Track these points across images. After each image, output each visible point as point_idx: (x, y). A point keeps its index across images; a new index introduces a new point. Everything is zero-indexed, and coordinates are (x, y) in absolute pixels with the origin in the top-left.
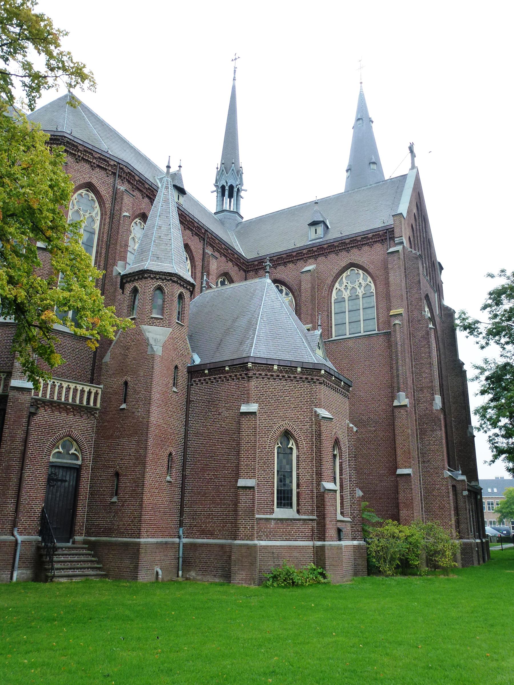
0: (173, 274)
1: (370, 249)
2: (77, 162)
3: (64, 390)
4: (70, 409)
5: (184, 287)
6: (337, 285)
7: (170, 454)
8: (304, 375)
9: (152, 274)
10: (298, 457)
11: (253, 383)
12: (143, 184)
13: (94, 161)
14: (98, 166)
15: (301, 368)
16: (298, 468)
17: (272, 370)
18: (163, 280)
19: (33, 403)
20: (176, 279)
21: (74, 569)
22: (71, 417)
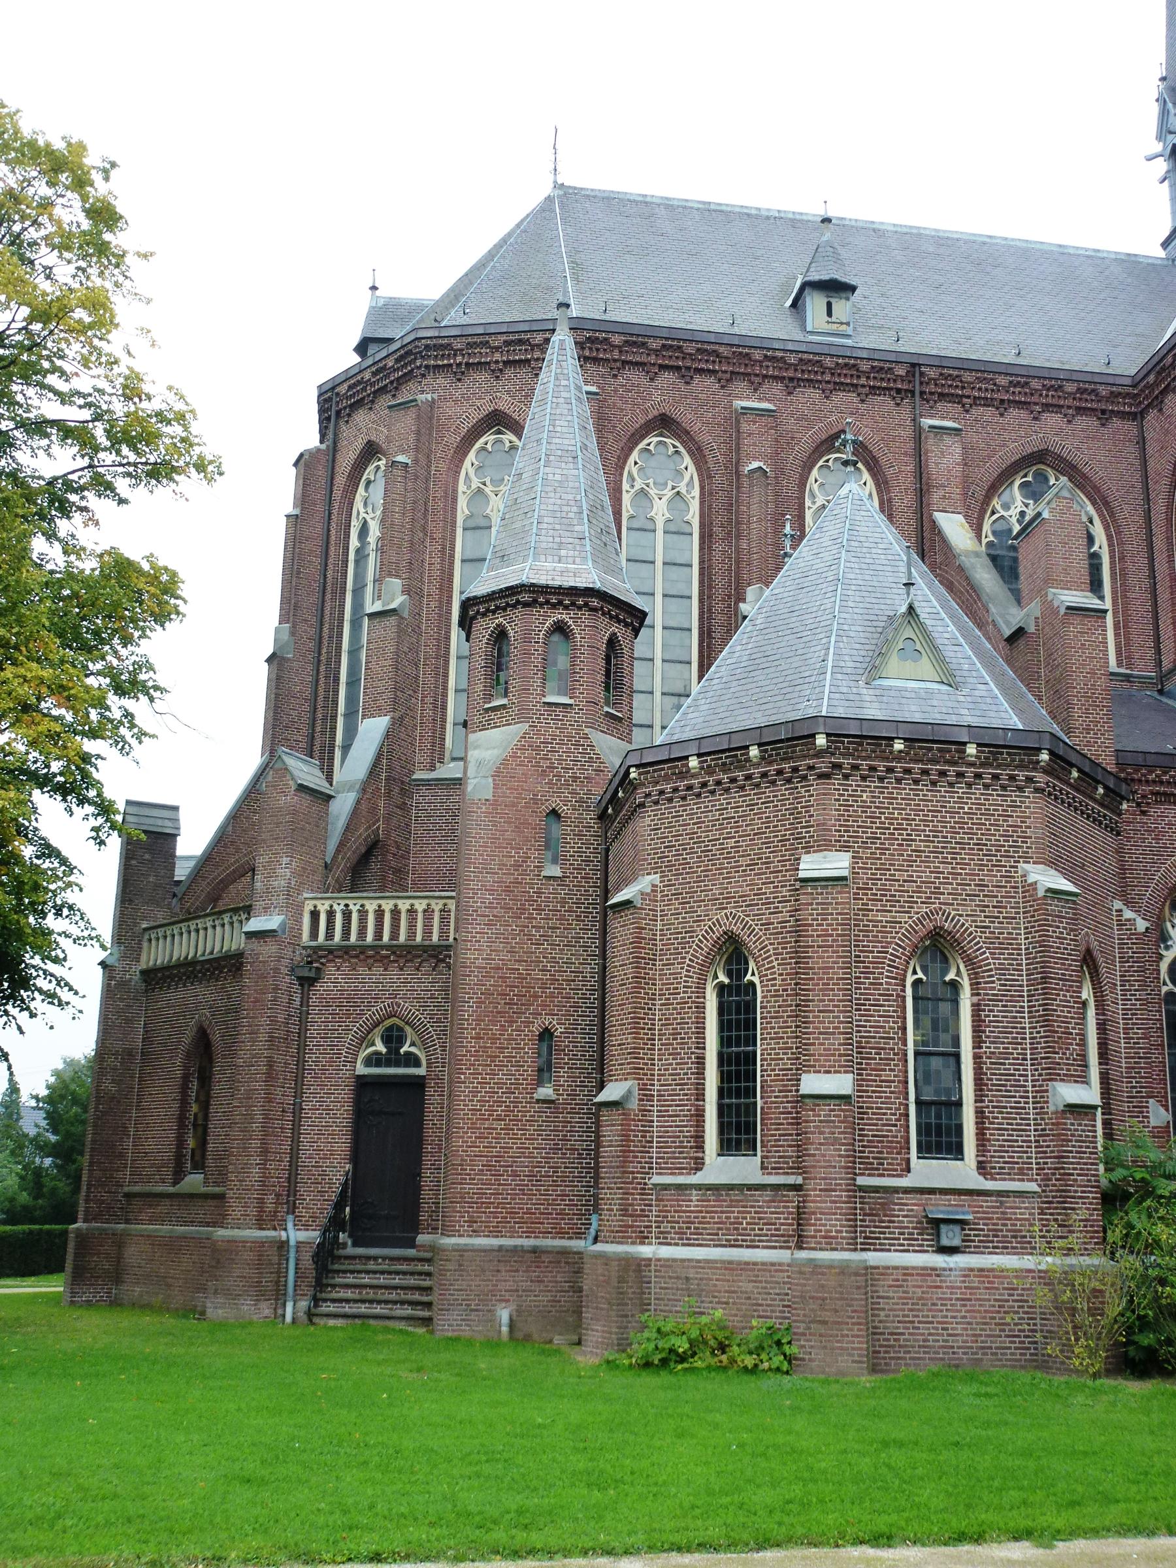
0: (517, 586)
1: (644, 381)
2: (459, 380)
3: (371, 918)
4: (388, 957)
5: (619, 621)
6: (996, 503)
7: (546, 1034)
8: (770, 763)
9: (481, 603)
10: (977, 1009)
11: (647, 821)
12: (644, 344)
13: (497, 356)
14: (507, 363)
15: (760, 745)
16: (977, 1043)
17: (685, 774)
18: (504, 609)
19: (308, 956)
20: (525, 597)
21: (371, 1302)
22: (394, 973)
